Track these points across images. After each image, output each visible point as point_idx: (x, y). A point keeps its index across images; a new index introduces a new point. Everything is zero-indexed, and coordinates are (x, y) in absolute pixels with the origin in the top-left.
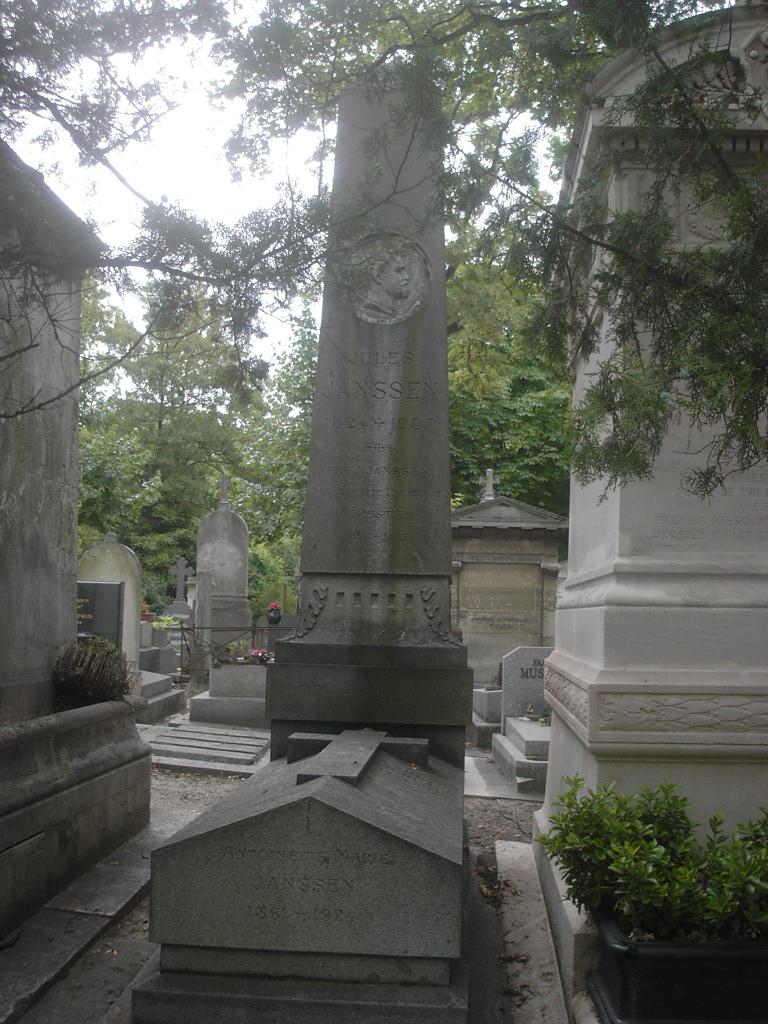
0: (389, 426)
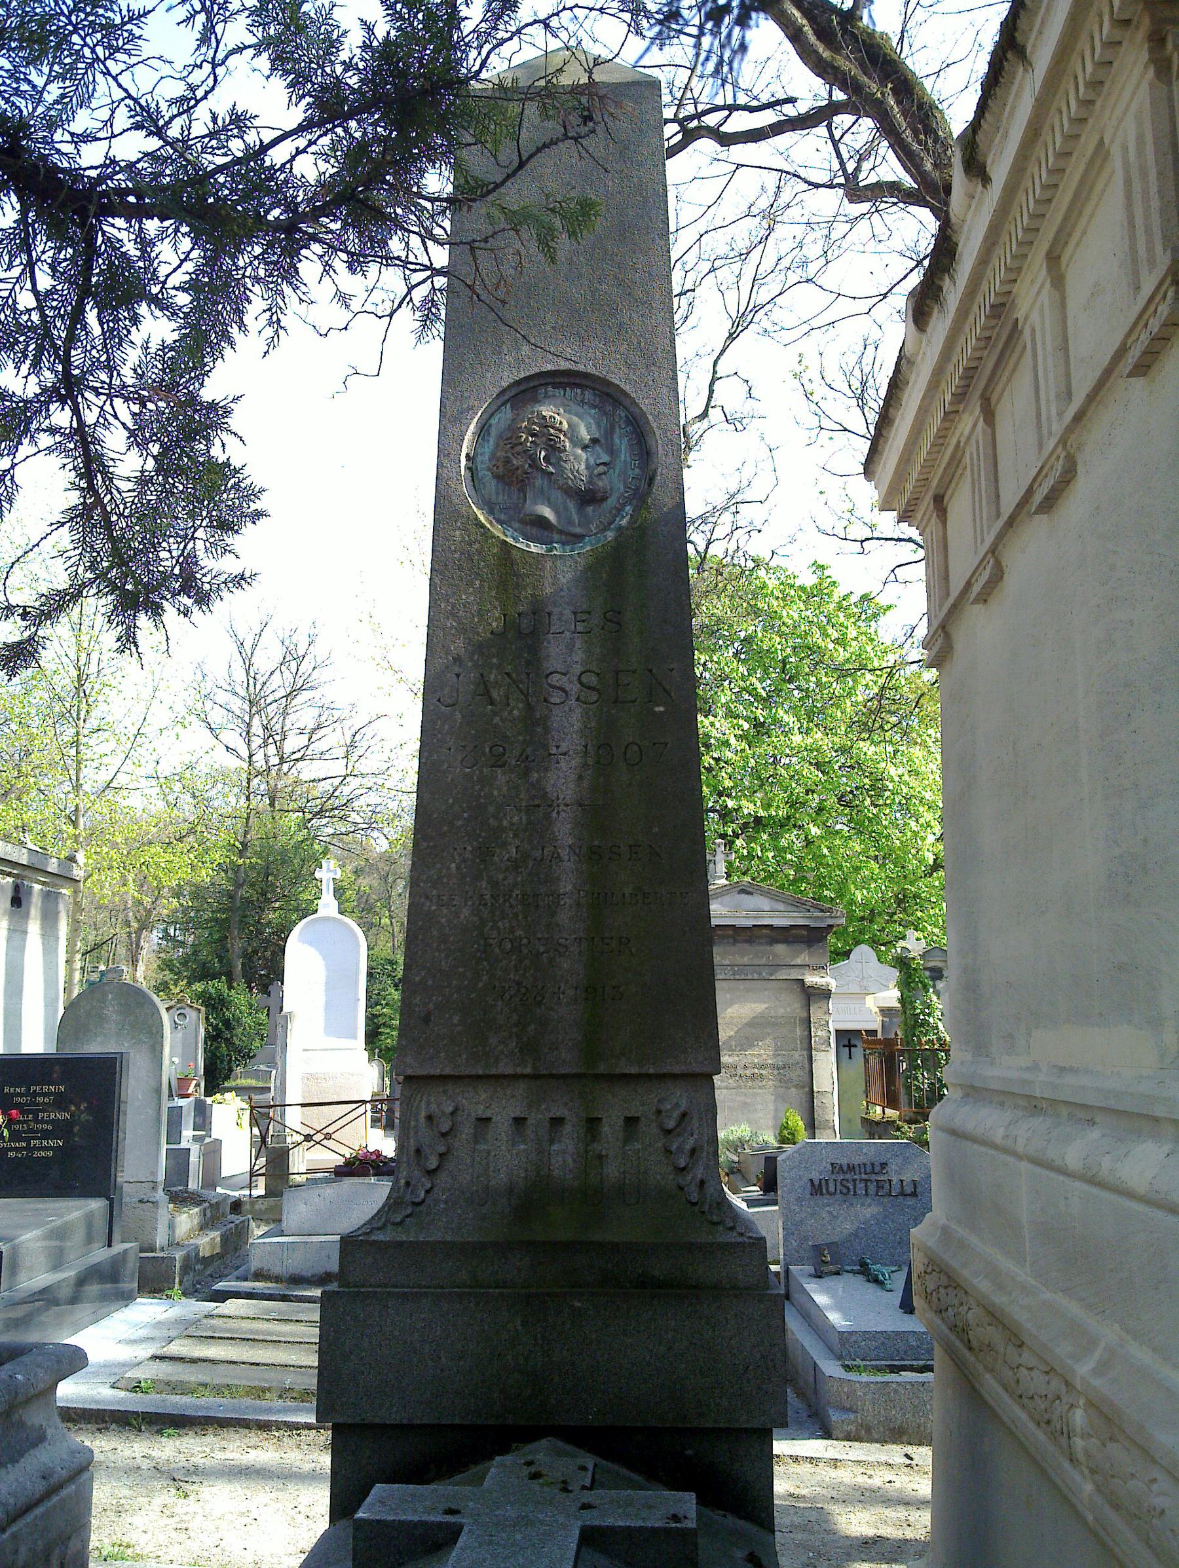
0: (576, 761)
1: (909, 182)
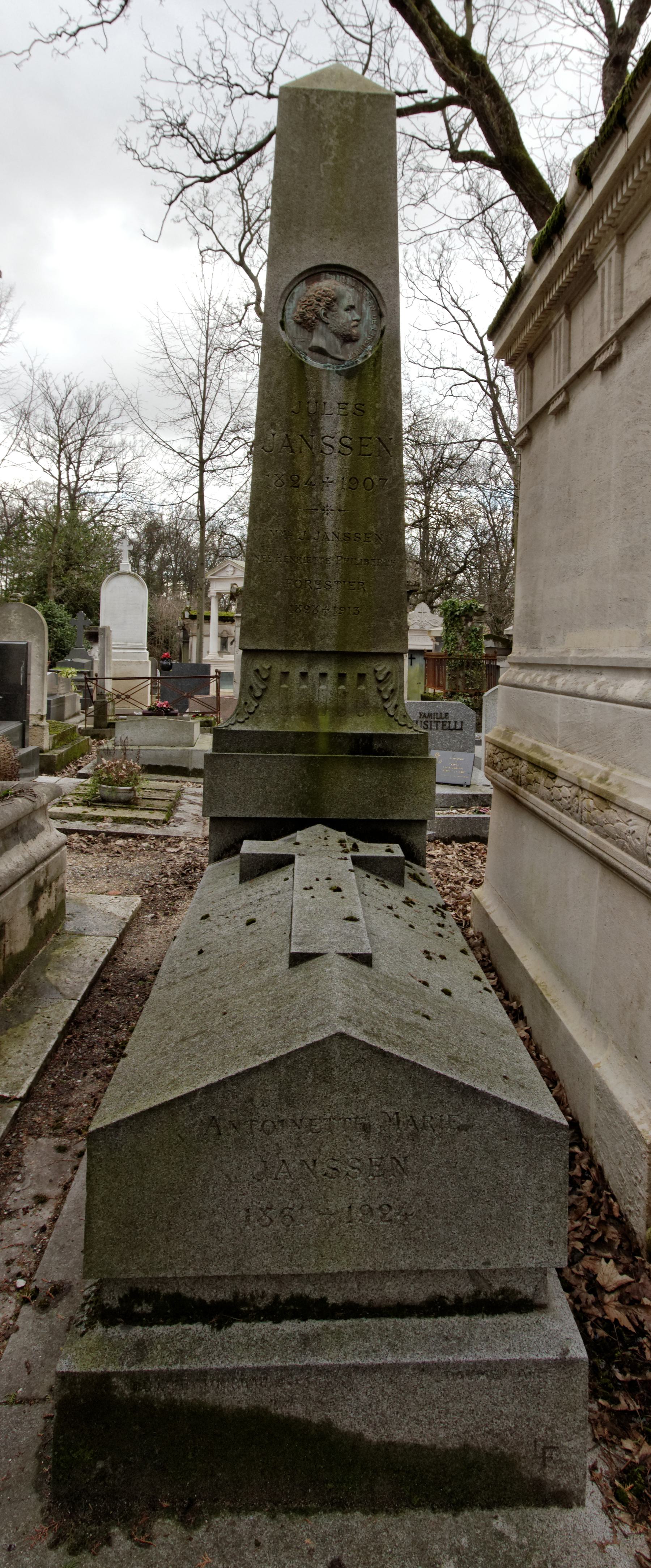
0: (339, 486)
1: (491, 154)
